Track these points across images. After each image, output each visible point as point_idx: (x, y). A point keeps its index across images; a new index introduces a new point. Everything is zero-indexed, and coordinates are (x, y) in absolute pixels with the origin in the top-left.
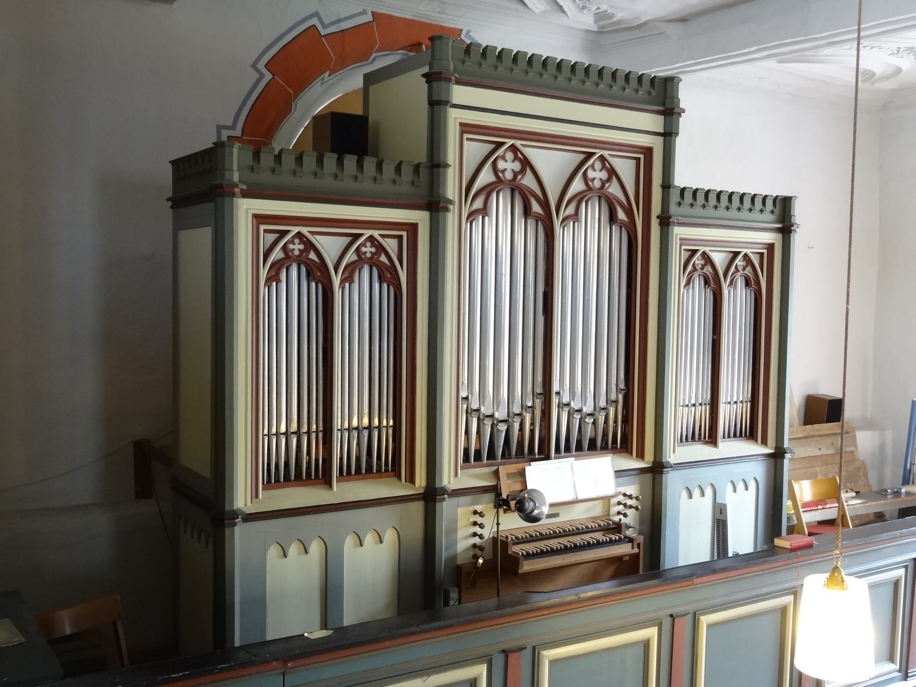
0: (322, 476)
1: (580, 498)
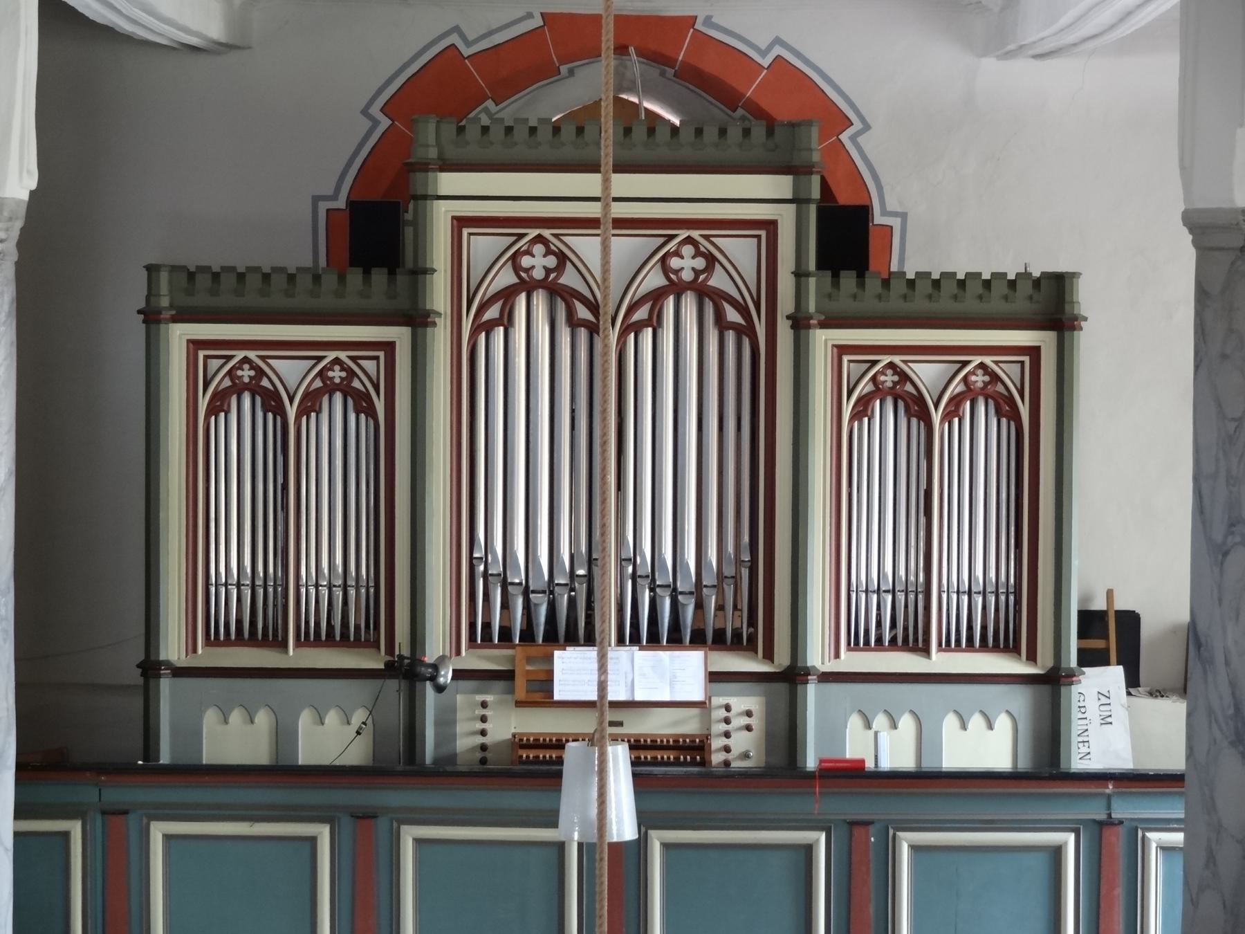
0: (917, 643)
1: (640, 696)
